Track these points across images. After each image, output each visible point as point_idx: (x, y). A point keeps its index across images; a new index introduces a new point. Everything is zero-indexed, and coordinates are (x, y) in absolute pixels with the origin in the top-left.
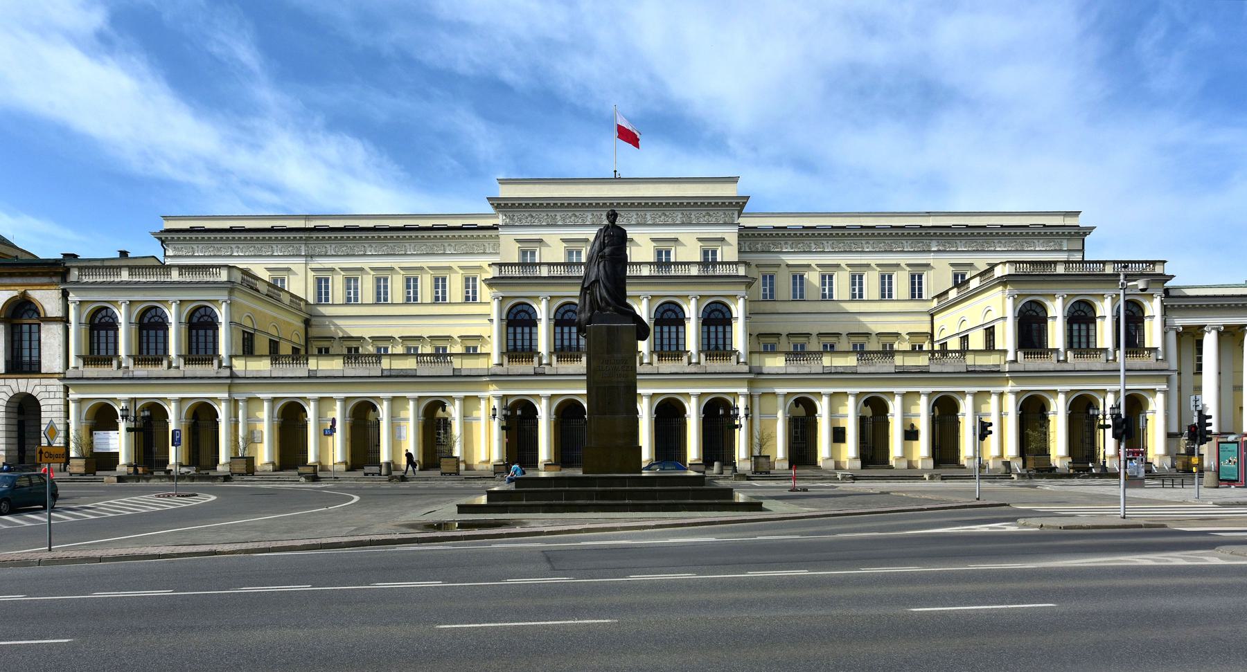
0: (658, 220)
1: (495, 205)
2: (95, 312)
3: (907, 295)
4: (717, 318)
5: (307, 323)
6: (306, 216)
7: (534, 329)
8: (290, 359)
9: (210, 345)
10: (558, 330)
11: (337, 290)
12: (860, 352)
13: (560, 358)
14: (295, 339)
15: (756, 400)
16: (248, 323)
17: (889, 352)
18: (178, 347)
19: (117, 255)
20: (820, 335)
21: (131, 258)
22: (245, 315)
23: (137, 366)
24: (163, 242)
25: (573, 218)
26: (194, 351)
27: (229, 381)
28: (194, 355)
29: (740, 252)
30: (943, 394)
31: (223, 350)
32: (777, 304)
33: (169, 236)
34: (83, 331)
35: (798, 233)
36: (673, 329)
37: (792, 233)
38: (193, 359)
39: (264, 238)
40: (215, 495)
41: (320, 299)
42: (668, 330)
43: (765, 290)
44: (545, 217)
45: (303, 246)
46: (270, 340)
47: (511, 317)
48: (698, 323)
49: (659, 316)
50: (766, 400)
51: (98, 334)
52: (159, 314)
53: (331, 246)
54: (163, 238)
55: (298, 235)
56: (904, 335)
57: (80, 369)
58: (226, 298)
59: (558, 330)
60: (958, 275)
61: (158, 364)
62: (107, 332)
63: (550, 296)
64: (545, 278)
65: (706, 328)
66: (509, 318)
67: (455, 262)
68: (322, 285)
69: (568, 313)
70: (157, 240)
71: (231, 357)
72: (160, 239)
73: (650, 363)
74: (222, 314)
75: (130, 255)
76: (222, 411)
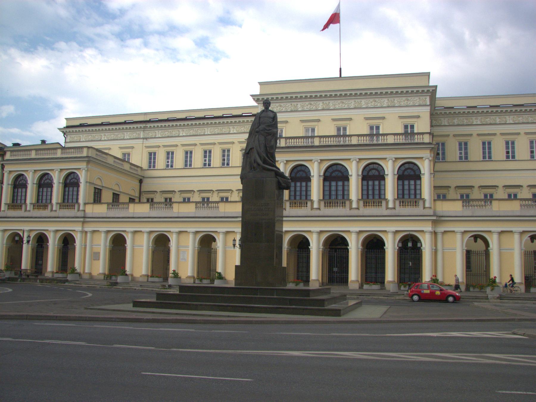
0: (402, 104)
1: (256, 99)
2: (17, 177)
3: (528, 156)
4: (374, 175)
5: (141, 181)
6: (145, 113)
7: (418, 182)
8: (201, 205)
9: (75, 197)
10: (365, 183)
11: (161, 161)
12: (466, 199)
13: (366, 204)
14: (132, 193)
15: (439, 237)
16: (98, 183)
17: (489, 199)
18: (32, 199)
19: (40, 143)
20: (506, 187)
21: (47, 144)
22: (97, 178)
23: (326, 207)
24: (64, 134)
25: (279, 107)
26: (66, 201)
27: (82, 220)
28: (40, 204)
29: (432, 126)
30: (159, 233)
31: (81, 200)
32: (471, 164)
33: (68, 130)
34: (61, 187)
35: (485, 110)
36: (412, 182)
37: (457, 111)
38: (66, 205)
39: (236, 122)
40: (11, 289)
41: (150, 167)
42: (76, 190)
43: (461, 153)
44: (290, 106)
45: (142, 132)
46: (114, 194)
47: (365, 173)
48: (431, 177)
49: (401, 173)
50: (447, 237)
51: (69, 189)
52: (49, 178)
53: (158, 132)
54: (65, 132)
55: (139, 126)
56: (196, 191)
57: (57, 211)
58: (429, 156)
59: (365, 183)
60: (126, 155)
61: (46, 209)
62: (301, 184)
63: (359, 159)
64: (283, 148)
65: (400, 182)
66: (325, 175)
67: (522, 129)
68: (152, 157)
69: (412, 171)
70: (61, 132)
71: (85, 204)
72: (63, 132)
73: (319, 209)
74: (83, 177)
75: (47, 143)
76: (78, 238)
